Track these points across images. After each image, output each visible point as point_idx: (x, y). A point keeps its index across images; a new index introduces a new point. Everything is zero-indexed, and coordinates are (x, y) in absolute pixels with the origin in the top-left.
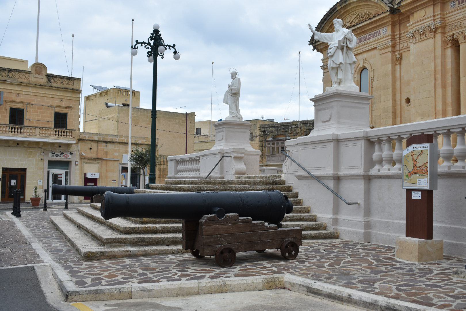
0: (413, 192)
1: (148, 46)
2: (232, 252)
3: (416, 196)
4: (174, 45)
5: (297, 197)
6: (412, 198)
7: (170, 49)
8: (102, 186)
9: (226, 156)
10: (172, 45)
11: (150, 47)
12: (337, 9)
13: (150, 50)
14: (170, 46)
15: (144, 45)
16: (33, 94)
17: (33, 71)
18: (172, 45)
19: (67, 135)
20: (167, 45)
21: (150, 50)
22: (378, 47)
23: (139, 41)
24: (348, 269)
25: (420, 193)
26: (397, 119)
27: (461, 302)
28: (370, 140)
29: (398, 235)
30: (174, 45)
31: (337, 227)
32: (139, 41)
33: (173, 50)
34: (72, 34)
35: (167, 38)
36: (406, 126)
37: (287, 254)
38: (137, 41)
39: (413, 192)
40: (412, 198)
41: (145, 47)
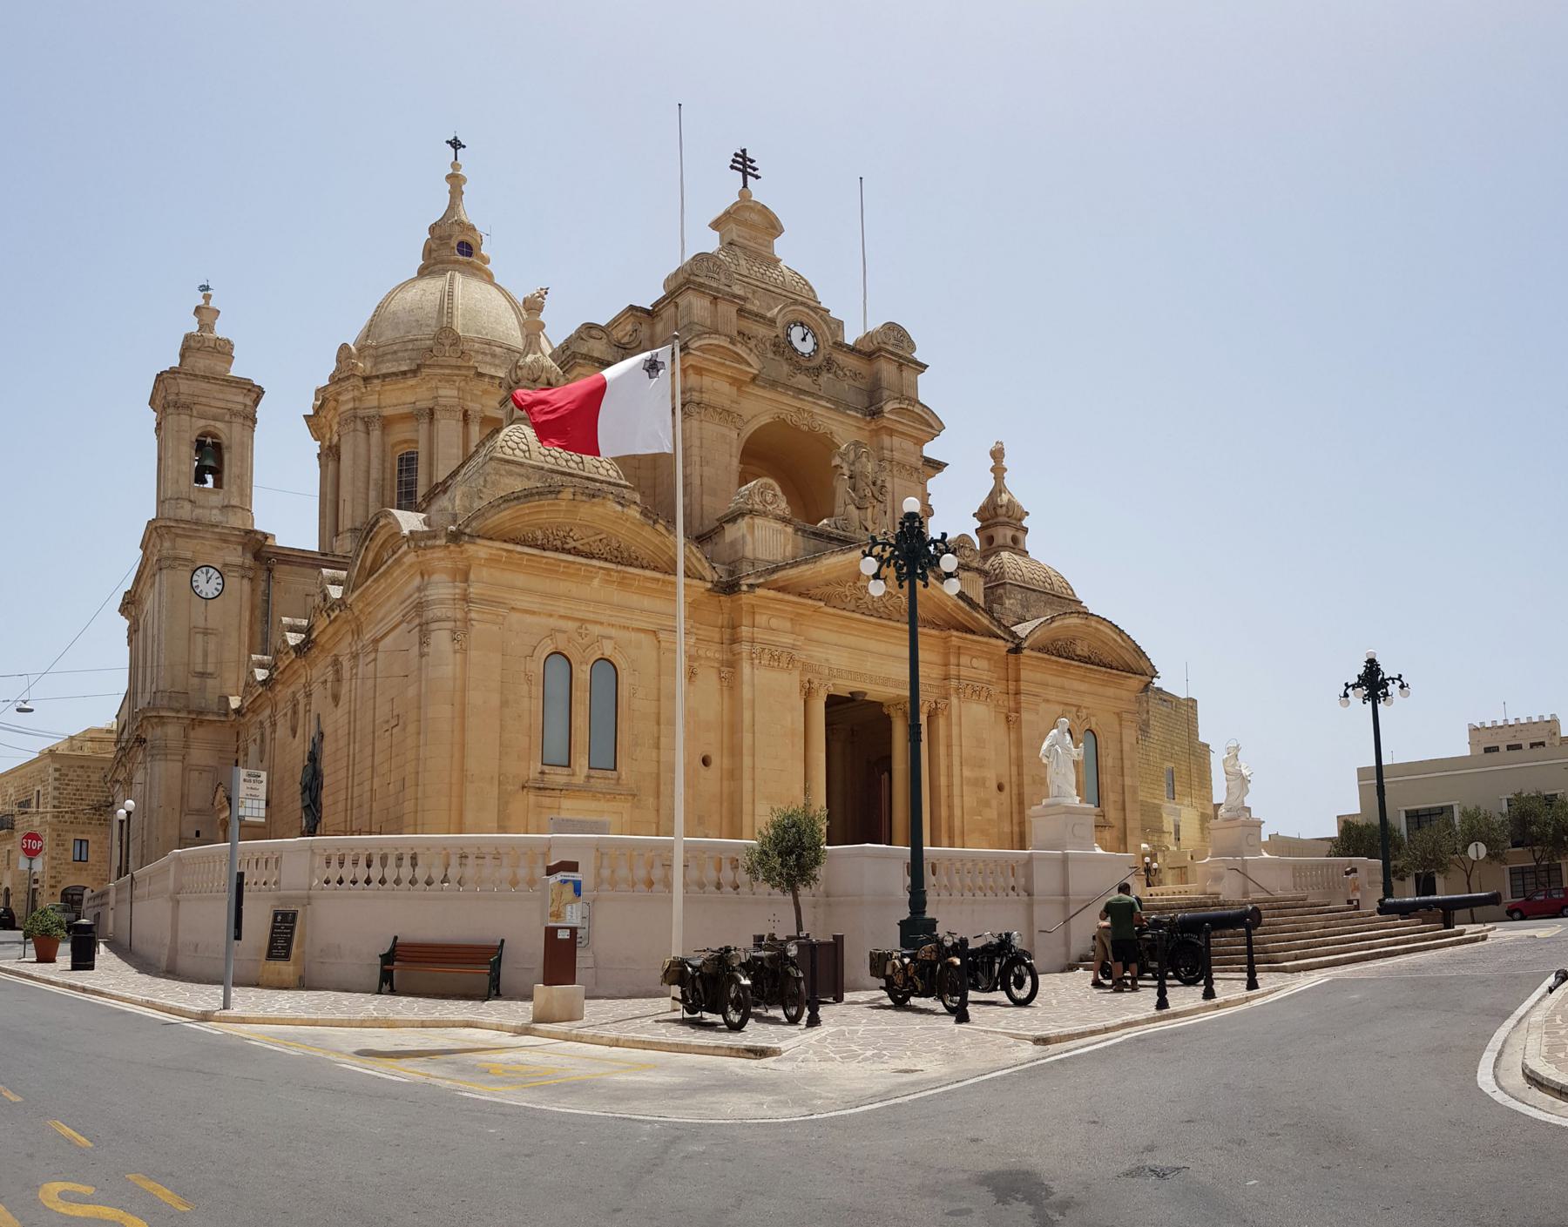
0: (559, 931)
3: (563, 935)
4: (1400, 676)
6: (559, 937)
7: (1394, 683)
10: (1397, 677)
14: (1393, 679)
18: (1397, 677)
20: (1390, 678)
23: (1349, 684)
25: (568, 931)
26: (946, 784)
27: (774, 1044)
29: (191, 1025)
30: (1400, 676)
31: (1411, 877)
32: (1349, 684)
33: (1398, 683)
34: (708, 753)
35: (1388, 670)
38: (1346, 684)
39: (559, 931)
40: (559, 937)
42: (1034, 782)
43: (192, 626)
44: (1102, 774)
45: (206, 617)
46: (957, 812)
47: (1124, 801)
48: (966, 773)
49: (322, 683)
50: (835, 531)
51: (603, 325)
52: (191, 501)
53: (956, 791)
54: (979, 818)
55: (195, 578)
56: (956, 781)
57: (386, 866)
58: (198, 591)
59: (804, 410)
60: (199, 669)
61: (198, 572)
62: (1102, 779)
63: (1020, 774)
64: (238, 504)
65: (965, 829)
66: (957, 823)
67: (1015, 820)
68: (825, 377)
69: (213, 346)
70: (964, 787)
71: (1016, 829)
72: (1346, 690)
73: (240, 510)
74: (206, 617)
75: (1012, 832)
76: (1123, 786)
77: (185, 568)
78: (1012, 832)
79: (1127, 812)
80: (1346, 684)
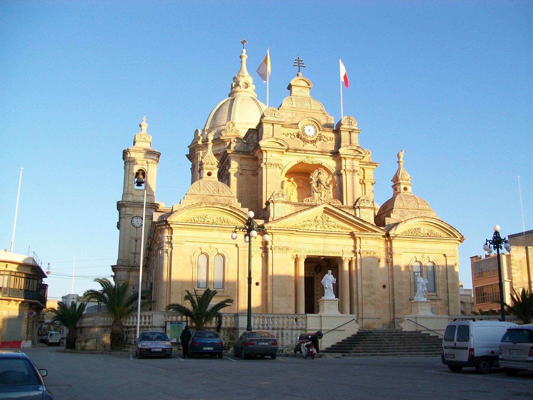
1: (244, 230)
2: (19, 343)
5: (324, 211)
8: (252, 244)
9: (126, 276)
11: (246, 231)
12: (201, 206)
13: (246, 233)
15: (241, 230)
16: (283, 243)
17: (475, 302)
19: (258, 327)
21: (246, 233)
22: (348, 235)
23: (488, 240)
24: (318, 212)
28: (376, 214)
32: (488, 240)
36: (351, 222)
37: (108, 287)
38: (487, 240)
41: (243, 230)
42: (399, 284)
43: (131, 237)
44: (436, 279)
45: (136, 234)
46: (360, 297)
47: (448, 289)
48: (364, 282)
49: (328, 186)
50: (308, 202)
51: (255, 128)
52: (132, 194)
53: (359, 289)
54: (370, 299)
55: (133, 220)
56: (359, 285)
57: (184, 331)
58: (134, 225)
59: (309, 157)
60: (134, 251)
61: (134, 219)
62: (436, 281)
63: (393, 281)
64: (149, 194)
65: (363, 302)
66: (360, 301)
67: (391, 299)
68: (318, 143)
69: (144, 138)
70: (363, 288)
71: (391, 302)
72: (487, 242)
73: (150, 196)
74: (136, 234)
75: (390, 303)
76: (448, 283)
77: (129, 217)
78: (390, 303)
79: (449, 293)
80: (487, 240)
